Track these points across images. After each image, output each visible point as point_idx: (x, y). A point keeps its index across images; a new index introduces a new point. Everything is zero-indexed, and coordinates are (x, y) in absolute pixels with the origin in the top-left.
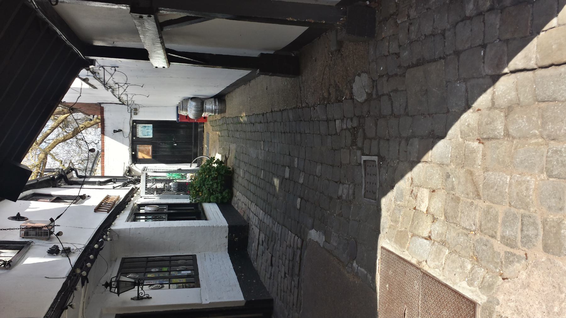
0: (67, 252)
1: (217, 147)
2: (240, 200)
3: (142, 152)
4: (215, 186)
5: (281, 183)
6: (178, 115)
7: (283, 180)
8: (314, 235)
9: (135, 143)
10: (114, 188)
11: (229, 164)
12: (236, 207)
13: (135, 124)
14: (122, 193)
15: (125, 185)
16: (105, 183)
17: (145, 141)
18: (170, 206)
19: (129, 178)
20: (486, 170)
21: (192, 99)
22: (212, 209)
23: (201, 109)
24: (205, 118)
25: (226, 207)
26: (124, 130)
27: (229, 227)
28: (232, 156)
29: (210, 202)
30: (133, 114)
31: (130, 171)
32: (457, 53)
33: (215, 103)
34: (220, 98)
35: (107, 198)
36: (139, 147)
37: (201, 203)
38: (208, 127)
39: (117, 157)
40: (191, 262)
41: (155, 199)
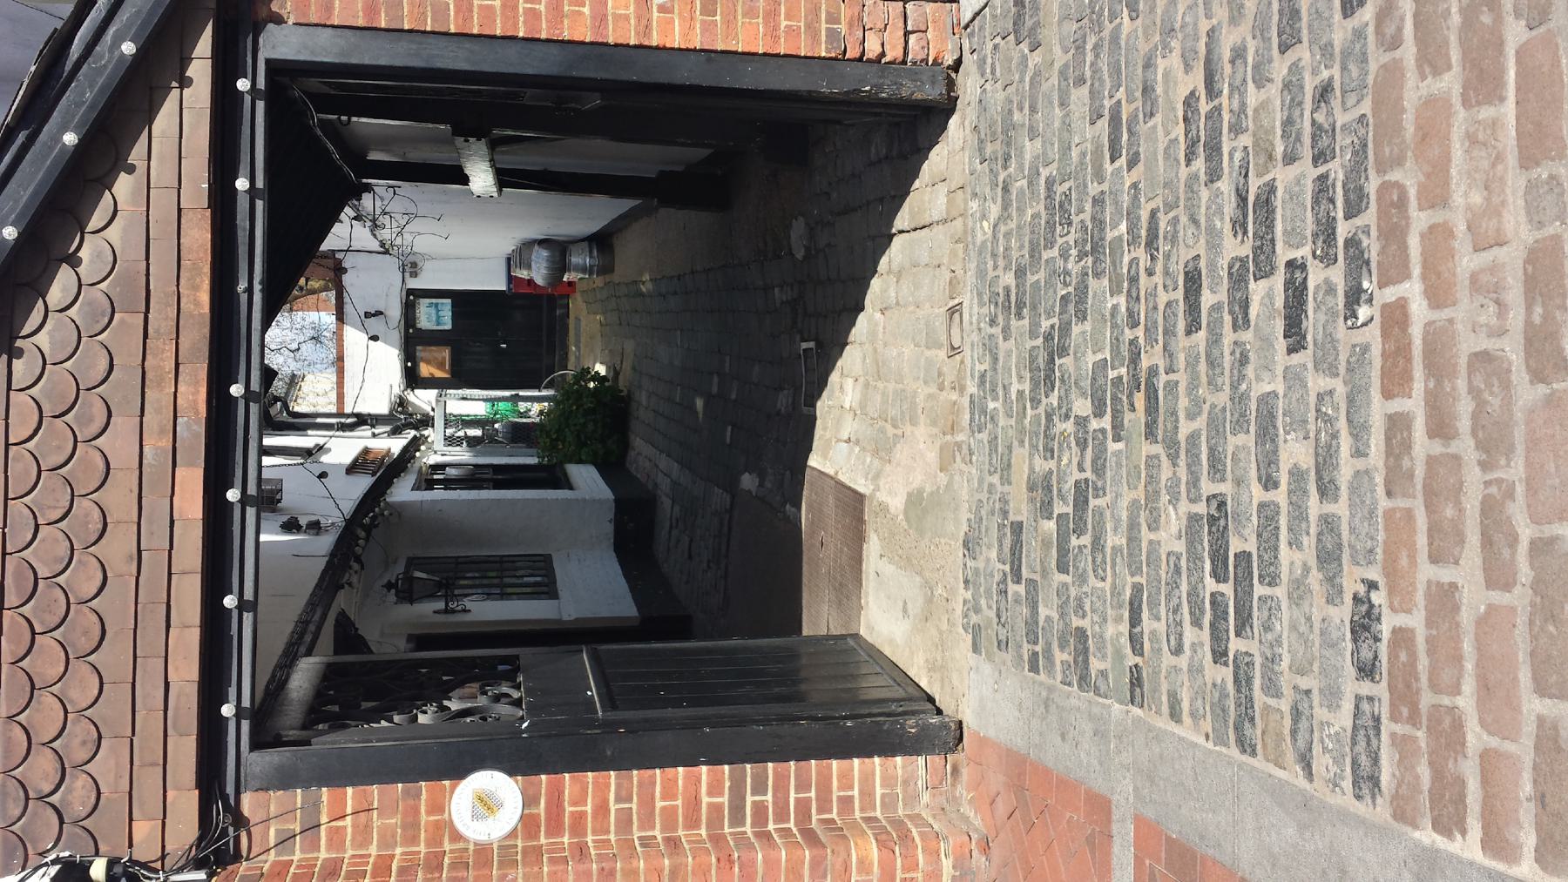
0: (315, 527)
1: (598, 351)
2: (647, 456)
3: (428, 362)
4: (591, 427)
5: (706, 406)
6: (511, 279)
7: (709, 399)
8: (748, 481)
9: (413, 342)
10: (374, 435)
11: (622, 383)
12: (633, 470)
13: (412, 298)
14: (396, 445)
15: (396, 432)
16: (352, 427)
17: (435, 338)
18: (497, 468)
19: (401, 418)
20: (885, 345)
21: (543, 243)
22: (586, 479)
23: (560, 265)
24: (570, 284)
25: (612, 467)
26: (387, 313)
27: (616, 501)
28: (627, 366)
29: (580, 462)
30: (407, 275)
31: (402, 403)
32: (868, 203)
33: (591, 252)
34: (601, 241)
35: (366, 451)
36: (421, 351)
37: (561, 464)
38: (577, 305)
39: (376, 372)
40: (543, 565)
41: (461, 455)
